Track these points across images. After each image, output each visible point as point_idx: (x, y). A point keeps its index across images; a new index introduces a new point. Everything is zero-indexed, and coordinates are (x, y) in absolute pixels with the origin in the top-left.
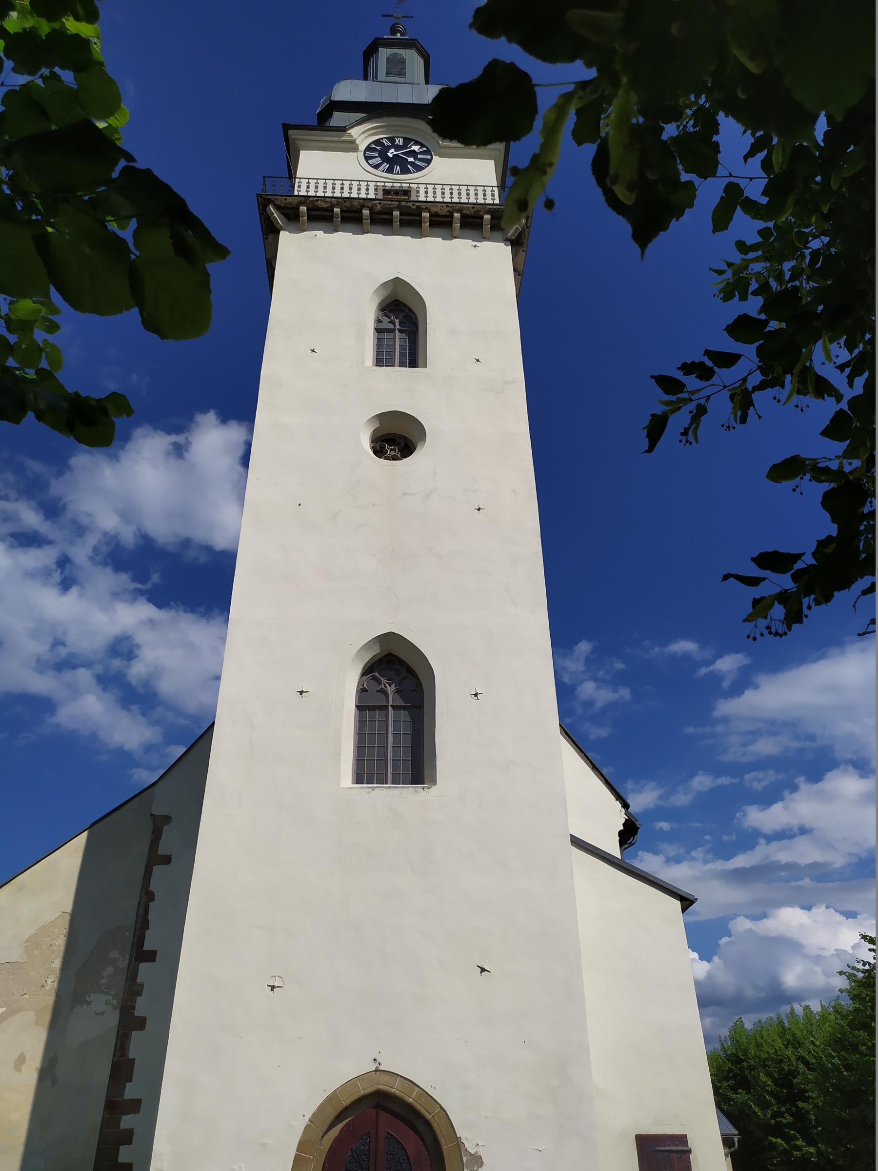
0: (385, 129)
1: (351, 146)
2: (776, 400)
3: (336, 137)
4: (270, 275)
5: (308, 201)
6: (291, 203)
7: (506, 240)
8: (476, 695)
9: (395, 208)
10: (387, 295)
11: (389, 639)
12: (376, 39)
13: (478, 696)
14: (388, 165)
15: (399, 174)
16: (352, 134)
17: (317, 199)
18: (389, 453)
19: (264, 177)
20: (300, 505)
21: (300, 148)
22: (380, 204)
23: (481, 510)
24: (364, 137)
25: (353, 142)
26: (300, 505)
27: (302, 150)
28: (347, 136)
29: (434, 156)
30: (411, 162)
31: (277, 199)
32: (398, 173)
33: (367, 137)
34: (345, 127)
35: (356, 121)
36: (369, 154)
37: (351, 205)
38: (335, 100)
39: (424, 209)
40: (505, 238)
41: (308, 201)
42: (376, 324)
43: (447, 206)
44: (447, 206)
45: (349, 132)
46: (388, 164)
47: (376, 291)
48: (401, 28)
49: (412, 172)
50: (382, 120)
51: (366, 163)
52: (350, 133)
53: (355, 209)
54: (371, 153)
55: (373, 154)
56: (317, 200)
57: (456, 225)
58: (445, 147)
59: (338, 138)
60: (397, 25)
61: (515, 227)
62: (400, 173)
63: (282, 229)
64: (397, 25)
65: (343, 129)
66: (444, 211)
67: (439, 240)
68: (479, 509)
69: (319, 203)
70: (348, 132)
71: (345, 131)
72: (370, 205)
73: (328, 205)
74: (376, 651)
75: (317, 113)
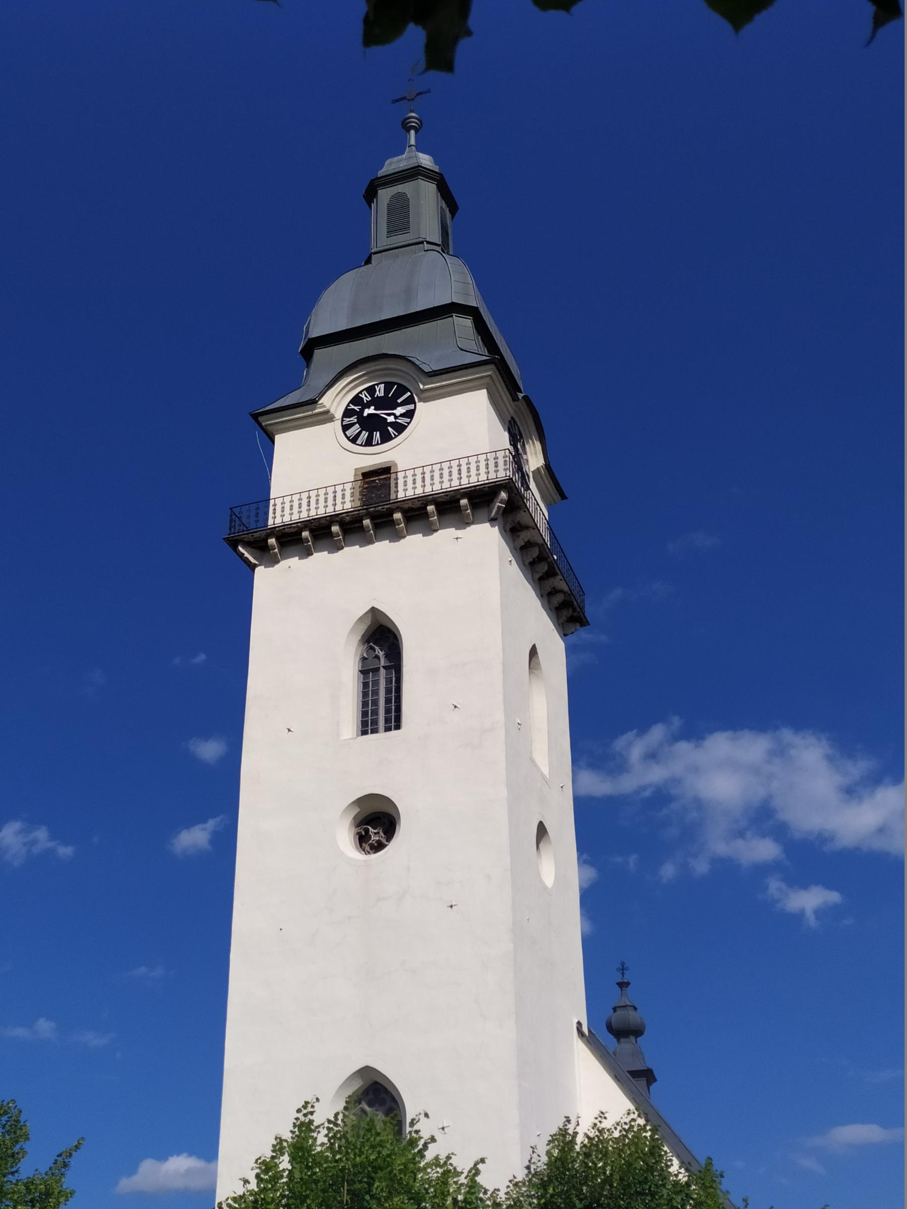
0: (366, 378)
1: (326, 417)
2: (303, 1109)
3: (308, 411)
4: (293, 525)
5: (275, 532)
6: (260, 537)
7: (492, 520)
8: (443, 1128)
9: (364, 515)
10: (366, 627)
11: (366, 1072)
12: (372, 181)
13: (445, 1129)
14: (378, 433)
15: (398, 436)
16: (325, 404)
17: (283, 527)
18: (372, 839)
19: (231, 509)
20: (281, 929)
21: (274, 433)
22: (348, 516)
23: (453, 907)
24: (340, 398)
25: (328, 412)
26: (281, 929)
27: (277, 434)
28: (320, 408)
29: (418, 404)
30: (391, 422)
31: (244, 538)
32: (396, 436)
33: (342, 397)
34: (315, 399)
35: (327, 386)
36: (347, 421)
37: (320, 524)
38: (313, 337)
39: (395, 509)
40: (490, 519)
41: (275, 532)
42: (361, 662)
43: (419, 501)
44: (419, 501)
45: (319, 403)
46: (367, 431)
47: (352, 630)
48: (413, 122)
49: (406, 424)
50: (358, 369)
51: (342, 433)
52: (322, 404)
53: (325, 525)
54: (349, 419)
55: (351, 419)
56: (284, 529)
57: (432, 519)
58: (426, 390)
59: (311, 413)
60: (408, 121)
61: (496, 506)
62: (397, 434)
63: (255, 566)
64: (408, 121)
65: (313, 402)
66: (418, 504)
67: (419, 536)
68: (451, 906)
69: (286, 530)
70: (319, 403)
71: (317, 402)
72: (338, 519)
73: (296, 529)
74: (357, 1085)
75: (299, 351)
